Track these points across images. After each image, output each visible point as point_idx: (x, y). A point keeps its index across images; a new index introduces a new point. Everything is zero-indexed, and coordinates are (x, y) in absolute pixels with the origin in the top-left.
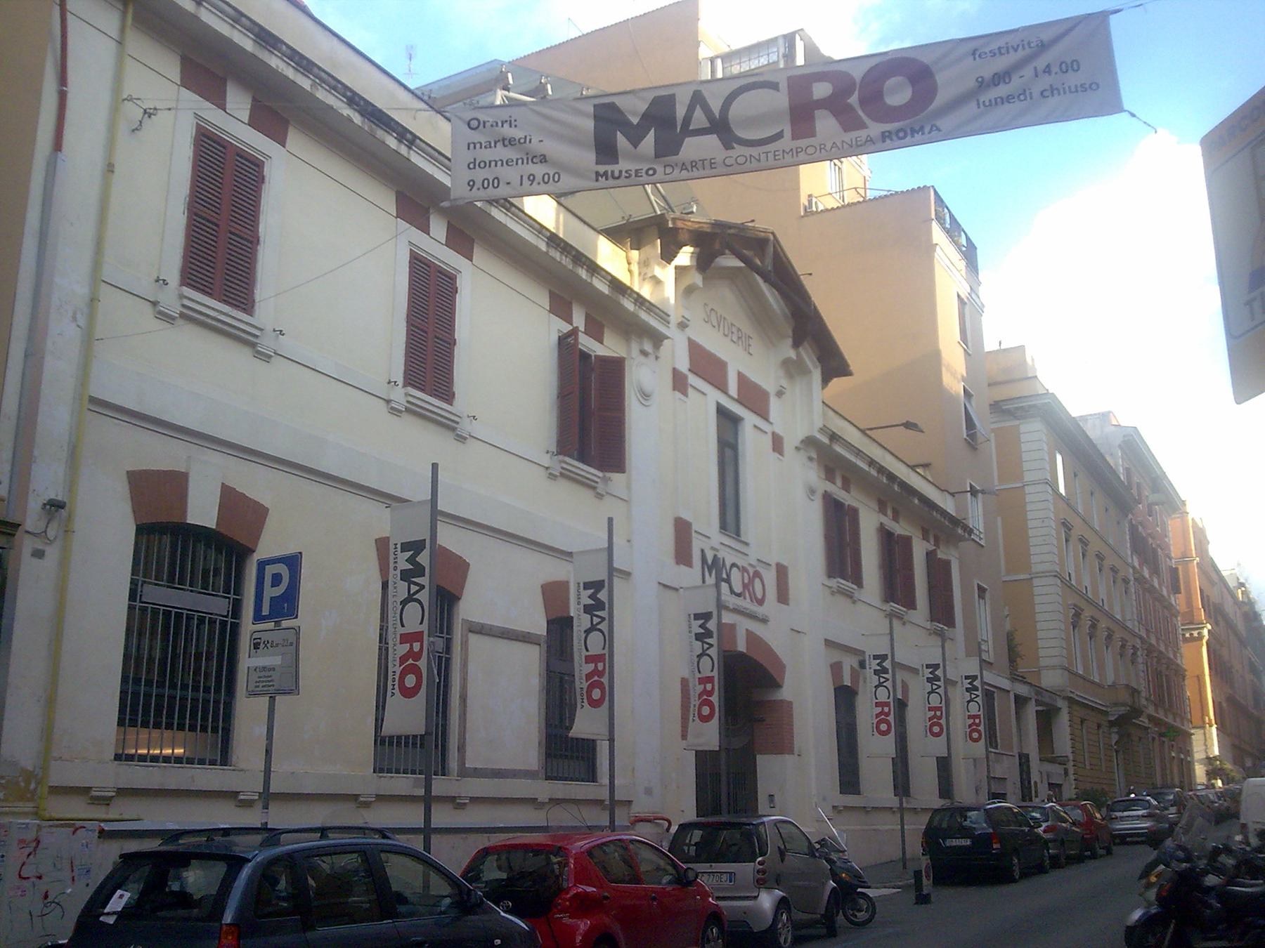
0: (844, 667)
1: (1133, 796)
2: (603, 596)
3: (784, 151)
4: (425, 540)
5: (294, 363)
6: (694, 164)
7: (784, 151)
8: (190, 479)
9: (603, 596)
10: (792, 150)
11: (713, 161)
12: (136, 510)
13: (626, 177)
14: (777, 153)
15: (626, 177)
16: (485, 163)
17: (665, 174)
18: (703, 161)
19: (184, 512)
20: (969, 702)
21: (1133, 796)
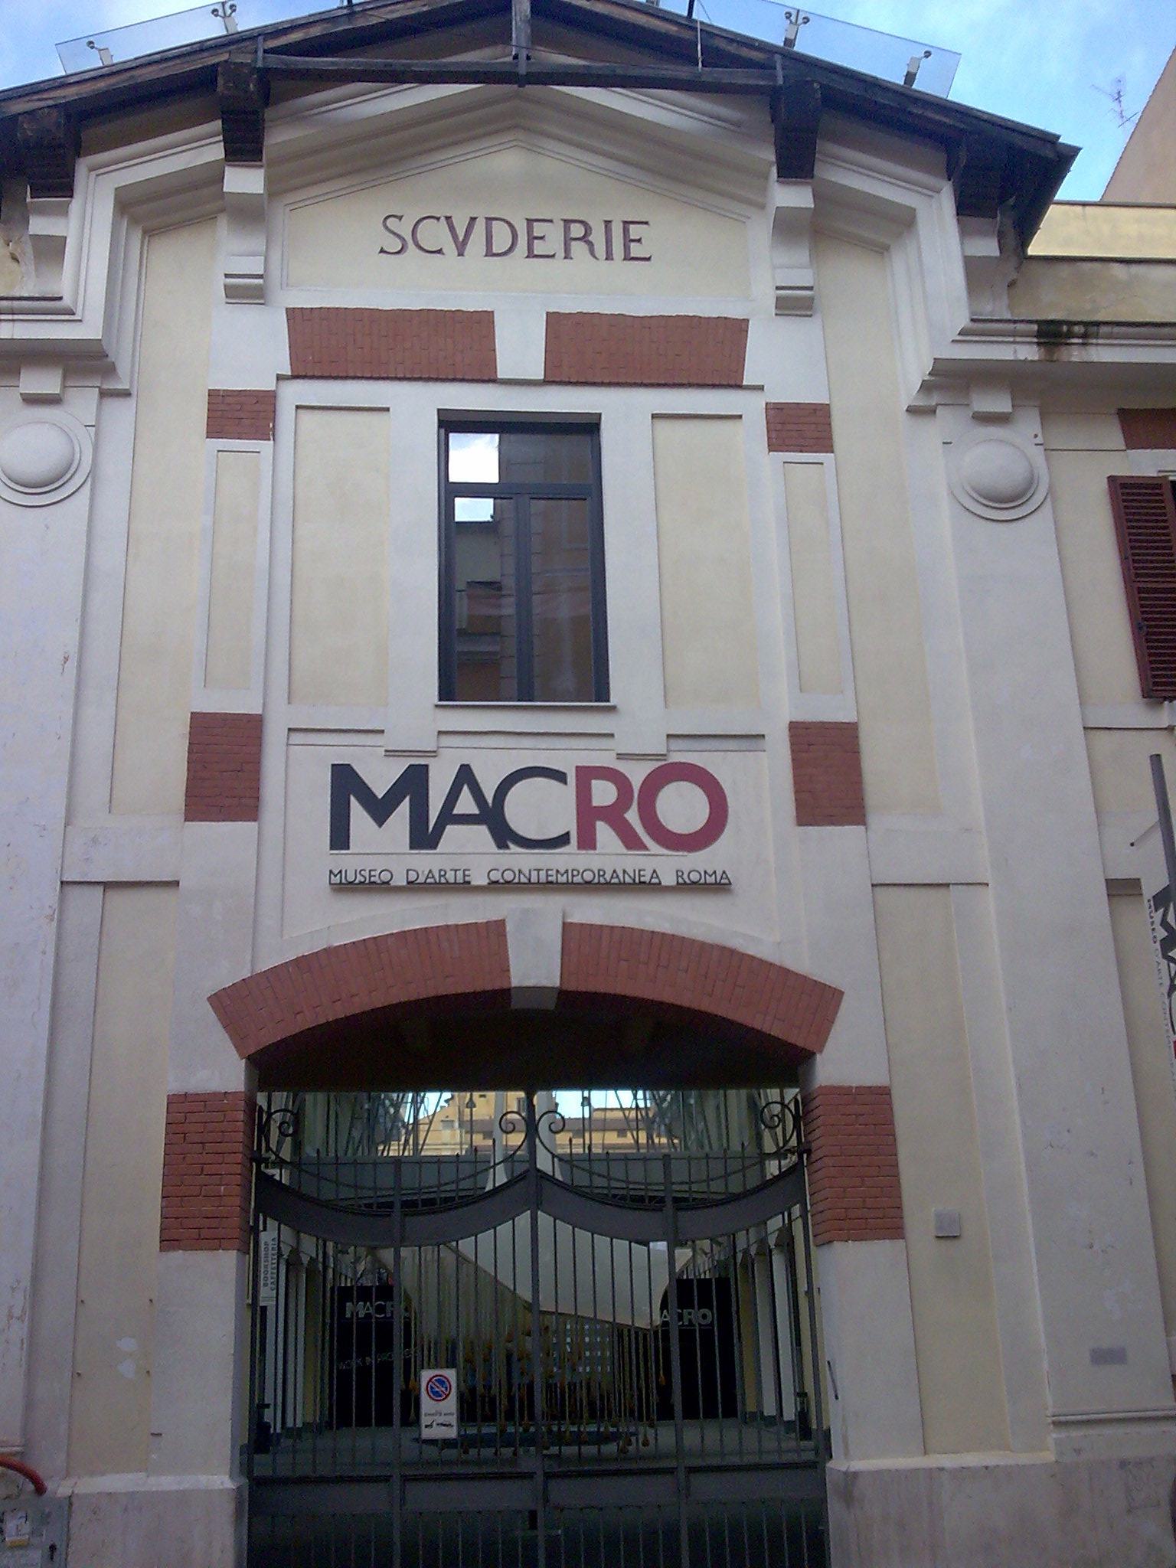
0: (576, 844)
1: (588, 1354)
2: (381, 778)
3: (558, 871)
4: (568, 834)
5: (890, 889)
6: (443, 873)
7: (558, 871)
8: (844, 1006)
9: (381, 778)
10: (340, 872)
11: (467, 873)
12: (239, 1046)
13: (365, 870)
14: (550, 872)
15: (365, 870)
16: (579, 872)
17: (408, 871)
18: (538, 870)
19: (510, 983)
20: (504, 835)
21: (588, 1354)
